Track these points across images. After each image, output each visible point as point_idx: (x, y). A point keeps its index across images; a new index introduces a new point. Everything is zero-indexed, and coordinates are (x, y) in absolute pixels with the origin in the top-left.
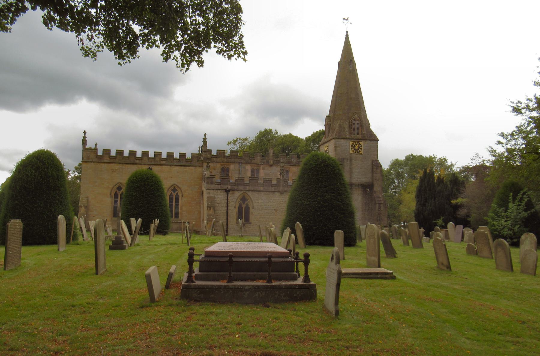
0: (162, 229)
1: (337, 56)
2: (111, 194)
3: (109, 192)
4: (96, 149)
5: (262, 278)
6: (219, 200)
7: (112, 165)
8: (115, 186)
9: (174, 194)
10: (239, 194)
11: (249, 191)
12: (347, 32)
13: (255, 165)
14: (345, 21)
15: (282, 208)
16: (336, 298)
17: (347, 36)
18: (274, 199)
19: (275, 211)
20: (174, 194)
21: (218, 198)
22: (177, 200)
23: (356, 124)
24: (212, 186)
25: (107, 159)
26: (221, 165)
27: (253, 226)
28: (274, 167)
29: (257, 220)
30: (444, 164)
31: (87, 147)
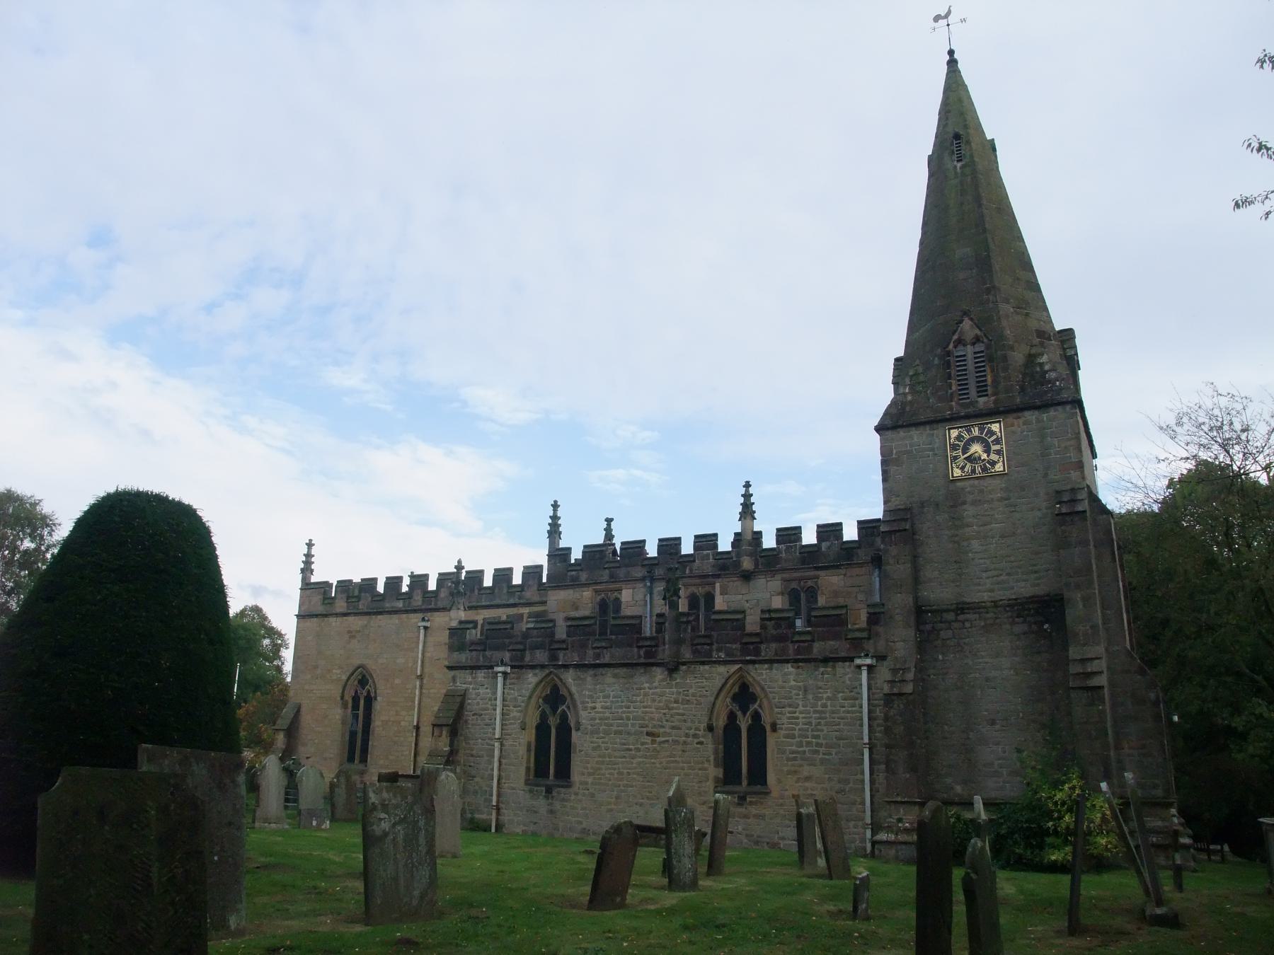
0: (801, 786)
2: (342, 698)
3: (337, 693)
6: (478, 704)
7: (351, 619)
8: (352, 674)
10: (539, 677)
11: (566, 667)
12: (951, 52)
13: (698, 581)
14: (943, 22)
15: (673, 728)
17: (952, 63)
18: (646, 695)
19: (649, 739)
21: (478, 694)
23: (970, 356)
26: (596, 591)
27: (576, 794)
28: (760, 582)
29: (589, 774)
31: (314, 579)
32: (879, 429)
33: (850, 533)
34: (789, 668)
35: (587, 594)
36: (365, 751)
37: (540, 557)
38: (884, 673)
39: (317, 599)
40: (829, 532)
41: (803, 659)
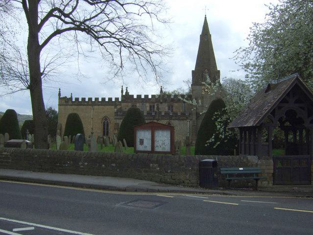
1: (200, 31)
4: (71, 98)
5: (187, 197)
9: (106, 122)
16: (43, 180)
17: (206, 18)
20: (106, 122)
22: (108, 126)
24: (118, 117)
25: (70, 103)
28: (164, 104)
30: (157, 99)
32: (219, 71)
33: (150, 97)
34: (177, 121)
35: (130, 104)
36: (108, 132)
37: (119, 96)
38: (191, 122)
39: (63, 101)
40: (146, 96)
41: (179, 120)
